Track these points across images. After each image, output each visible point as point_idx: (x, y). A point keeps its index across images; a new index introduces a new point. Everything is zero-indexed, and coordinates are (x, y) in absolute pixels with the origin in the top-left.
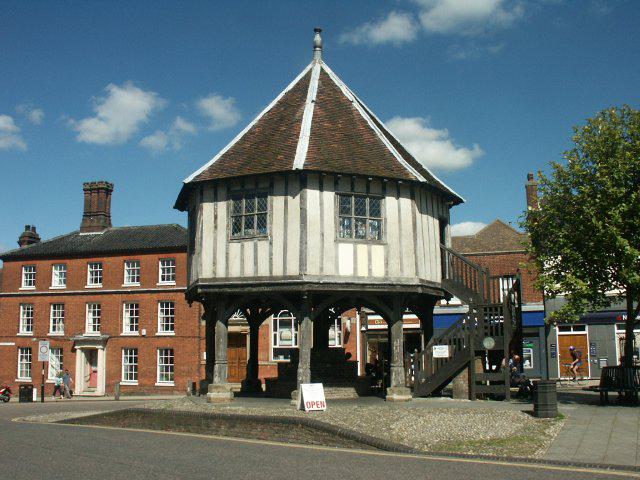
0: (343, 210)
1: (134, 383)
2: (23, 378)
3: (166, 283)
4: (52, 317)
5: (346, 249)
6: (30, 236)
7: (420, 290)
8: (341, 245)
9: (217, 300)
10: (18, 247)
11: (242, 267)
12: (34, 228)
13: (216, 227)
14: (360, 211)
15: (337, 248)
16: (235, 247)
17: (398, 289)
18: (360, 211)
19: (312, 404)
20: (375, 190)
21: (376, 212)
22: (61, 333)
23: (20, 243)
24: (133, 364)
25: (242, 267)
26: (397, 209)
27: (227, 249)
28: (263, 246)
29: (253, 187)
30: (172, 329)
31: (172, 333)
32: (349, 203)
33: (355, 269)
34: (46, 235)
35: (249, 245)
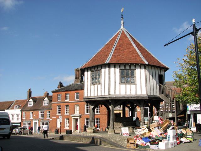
0: (122, 76)
2: (59, 126)
3: (77, 99)
4: (66, 109)
5: (123, 86)
6: (61, 85)
7: (147, 98)
8: (121, 85)
9: (95, 103)
11: (109, 91)
12: (62, 83)
13: (88, 81)
14: (128, 74)
15: (120, 86)
16: (92, 86)
17: (140, 98)
18: (128, 74)
19: (125, 134)
20: (133, 68)
21: (133, 74)
22: (68, 114)
23: (58, 87)
24: (26, 126)
25: (109, 91)
26: (140, 73)
27: (91, 87)
28: (99, 86)
29: (93, 70)
30: (99, 112)
31: (89, 114)
32: (124, 72)
33: (126, 92)
34: (65, 85)
35: (96, 86)
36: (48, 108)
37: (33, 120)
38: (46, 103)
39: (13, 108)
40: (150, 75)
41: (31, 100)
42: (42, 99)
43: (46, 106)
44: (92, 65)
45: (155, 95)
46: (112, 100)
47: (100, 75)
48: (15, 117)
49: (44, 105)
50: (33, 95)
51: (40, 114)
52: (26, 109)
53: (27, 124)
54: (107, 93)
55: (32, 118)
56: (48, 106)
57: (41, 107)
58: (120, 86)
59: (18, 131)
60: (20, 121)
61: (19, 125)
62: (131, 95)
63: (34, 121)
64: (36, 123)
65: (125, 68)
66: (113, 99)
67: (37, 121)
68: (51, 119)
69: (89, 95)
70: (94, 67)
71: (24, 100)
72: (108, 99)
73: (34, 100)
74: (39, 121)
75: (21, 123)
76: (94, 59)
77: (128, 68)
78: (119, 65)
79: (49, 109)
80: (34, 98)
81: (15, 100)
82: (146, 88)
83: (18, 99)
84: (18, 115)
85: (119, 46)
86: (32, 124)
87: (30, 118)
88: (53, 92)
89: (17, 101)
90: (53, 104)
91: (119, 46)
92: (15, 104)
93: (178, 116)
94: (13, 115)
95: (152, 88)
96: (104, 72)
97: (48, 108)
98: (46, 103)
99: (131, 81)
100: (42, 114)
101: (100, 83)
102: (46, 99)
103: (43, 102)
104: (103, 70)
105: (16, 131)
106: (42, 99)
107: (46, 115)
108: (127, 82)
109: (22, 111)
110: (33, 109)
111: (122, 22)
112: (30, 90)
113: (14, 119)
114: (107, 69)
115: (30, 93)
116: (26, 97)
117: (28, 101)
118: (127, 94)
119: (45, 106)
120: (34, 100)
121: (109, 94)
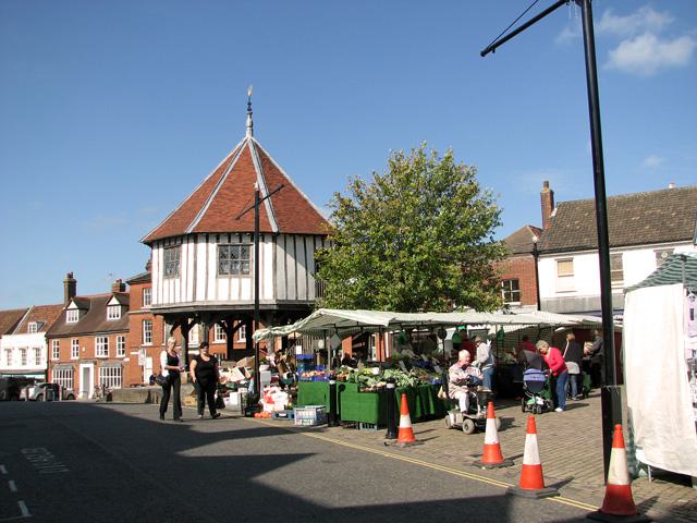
0: (222, 256)
1: (150, 344)
5: (224, 281)
7: (275, 307)
10: (145, 271)
16: (166, 282)
28: (178, 281)
35: (172, 281)
36: (120, 329)
37: (79, 362)
38: (113, 312)
39: (24, 331)
40: (288, 256)
41: (73, 305)
42: (103, 303)
43: (115, 321)
44: (168, 234)
45: (302, 298)
46: (199, 312)
47: (179, 257)
48: (31, 354)
49: (108, 318)
50: (80, 293)
51: (98, 345)
52: (60, 332)
53: (63, 374)
54: (190, 299)
55: (77, 358)
56: (119, 322)
57: (104, 323)
58: (217, 281)
59: (36, 392)
60: (44, 366)
61: (42, 377)
62: (240, 300)
63: (82, 366)
64: (87, 370)
65: (229, 241)
66: (200, 309)
67: (91, 366)
68: (127, 360)
69: (160, 302)
70: (169, 239)
71: (52, 307)
72: (192, 309)
73: (84, 305)
74: (95, 363)
75: (46, 372)
76: (171, 221)
77: (235, 241)
78: (218, 236)
79: (120, 331)
80: (83, 299)
81: (31, 307)
82: (275, 285)
83: (39, 303)
84: (38, 350)
85: (228, 188)
86: (78, 375)
87: (73, 358)
88: (131, 283)
89: (36, 309)
90: (131, 317)
91: (228, 188)
92: (29, 319)
93: (356, 346)
94: (24, 350)
95: (291, 283)
96: (187, 248)
97: (120, 329)
98: (113, 312)
99: (242, 270)
100: (104, 344)
101: (179, 276)
102: (114, 301)
103: (106, 313)
104: (184, 246)
105: (28, 393)
106: (103, 303)
107: (113, 347)
108: (233, 272)
109: (48, 338)
110: (79, 332)
111: (249, 121)
112: (70, 276)
113: (27, 362)
114: (192, 245)
115: (71, 286)
116: (59, 297)
117: (67, 309)
118: (209, 299)
119: (111, 323)
120: (84, 305)
121: (194, 301)
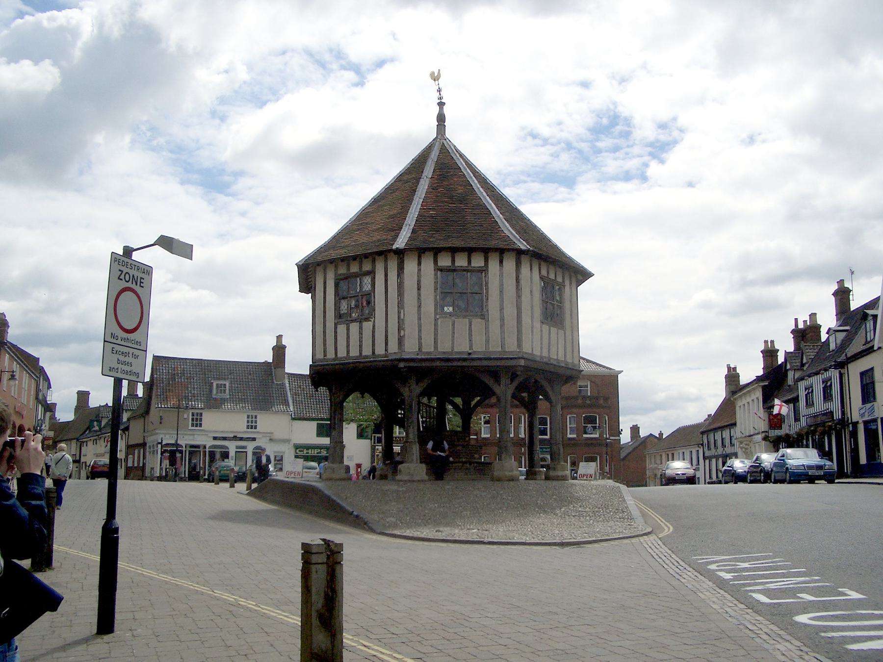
16: (445, 326)
